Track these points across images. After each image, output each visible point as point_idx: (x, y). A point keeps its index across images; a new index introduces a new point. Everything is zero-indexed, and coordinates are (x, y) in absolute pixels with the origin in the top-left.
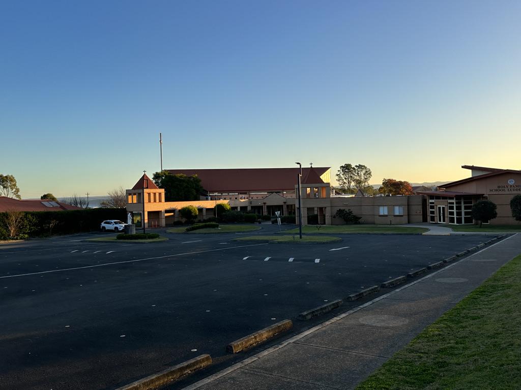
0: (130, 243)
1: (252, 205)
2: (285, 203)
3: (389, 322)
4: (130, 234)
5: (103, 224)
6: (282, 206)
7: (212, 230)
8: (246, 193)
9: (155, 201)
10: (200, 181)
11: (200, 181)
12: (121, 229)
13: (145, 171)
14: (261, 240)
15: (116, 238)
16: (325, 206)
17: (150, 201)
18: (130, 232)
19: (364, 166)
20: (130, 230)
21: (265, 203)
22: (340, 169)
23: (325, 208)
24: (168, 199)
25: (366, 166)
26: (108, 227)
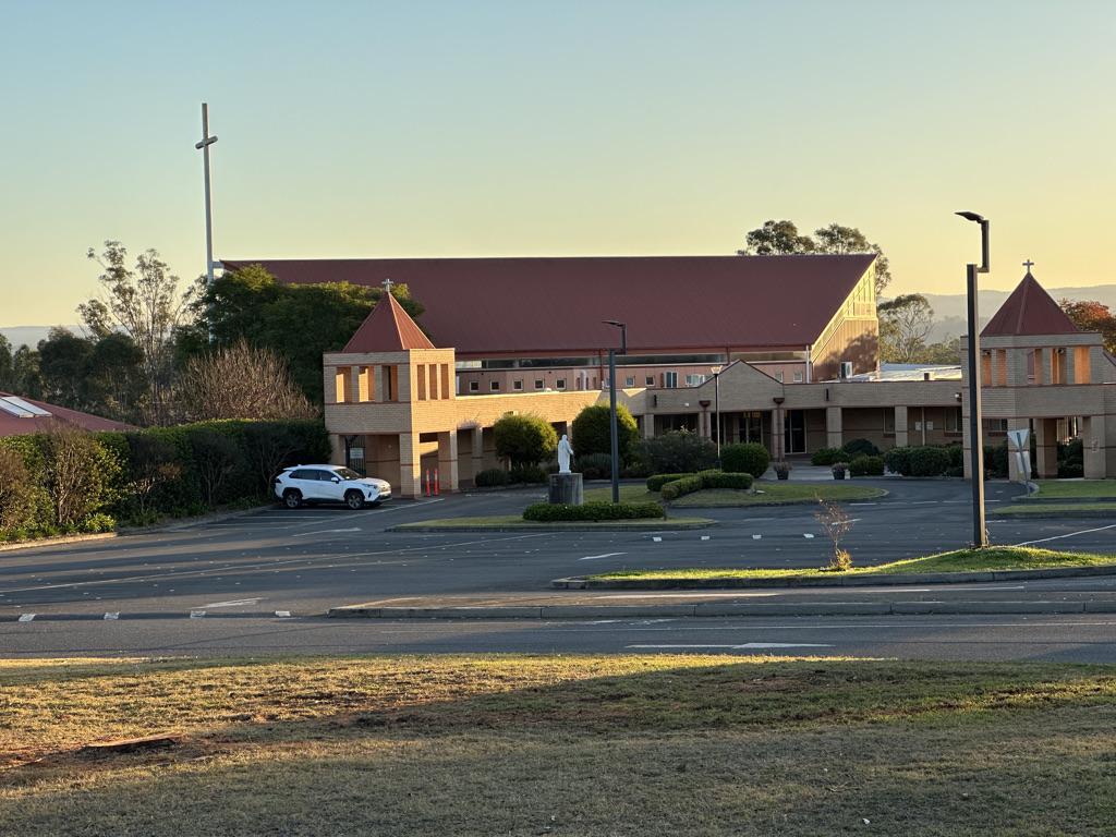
0: (626, 528)
1: (661, 410)
2: (779, 401)
3: (1086, 753)
4: (574, 503)
5: (286, 480)
6: (767, 415)
7: (741, 497)
8: (582, 363)
9: (434, 397)
10: (1107, 308)
11: (1107, 308)
12: (373, 498)
13: (1029, 264)
14: (1102, 512)
15: (521, 517)
16: (1086, 413)
17: (422, 397)
18: (574, 498)
19: (856, 235)
20: (573, 493)
21: (705, 404)
22: (123, 254)
23: (1086, 418)
24: (470, 385)
25: (862, 233)
26: (310, 489)
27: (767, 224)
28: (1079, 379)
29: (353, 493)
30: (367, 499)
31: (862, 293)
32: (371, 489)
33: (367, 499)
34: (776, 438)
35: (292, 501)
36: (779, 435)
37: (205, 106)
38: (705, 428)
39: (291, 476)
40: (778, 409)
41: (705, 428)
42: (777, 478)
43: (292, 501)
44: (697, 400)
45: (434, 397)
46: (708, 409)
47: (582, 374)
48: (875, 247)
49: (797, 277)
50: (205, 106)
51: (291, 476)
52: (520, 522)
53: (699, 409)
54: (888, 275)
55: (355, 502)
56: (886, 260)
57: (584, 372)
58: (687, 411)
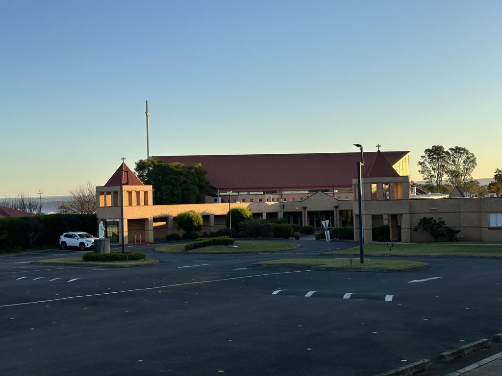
0: (103, 266)
1: (286, 210)
2: (336, 207)
5: (63, 238)
7: (225, 249)
9: (138, 204)
12: (89, 246)
17: (130, 204)
18: (102, 250)
21: (305, 208)
25: (467, 149)
26: (70, 242)
27: (433, 147)
28: (399, 198)
29: (82, 244)
30: (86, 246)
31: (401, 166)
32: (88, 242)
33: (86, 246)
34: (306, 220)
35: (64, 247)
36: (337, 220)
37: (147, 101)
38: (305, 217)
39: (64, 237)
40: (336, 210)
41: (305, 217)
42: (315, 239)
43: (64, 247)
44: (301, 206)
45: (138, 204)
46: (306, 210)
47: (270, 197)
48: (472, 154)
49: (382, 163)
50: (147, 101)
51: (64, 237)
52: (80, 261)
53: (302, 210)
54: (476, 163)
55: (82, 248)
56: (475, 158)
57: (271, 196)
58: (297, 211)
